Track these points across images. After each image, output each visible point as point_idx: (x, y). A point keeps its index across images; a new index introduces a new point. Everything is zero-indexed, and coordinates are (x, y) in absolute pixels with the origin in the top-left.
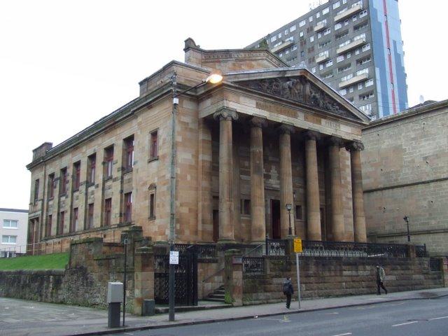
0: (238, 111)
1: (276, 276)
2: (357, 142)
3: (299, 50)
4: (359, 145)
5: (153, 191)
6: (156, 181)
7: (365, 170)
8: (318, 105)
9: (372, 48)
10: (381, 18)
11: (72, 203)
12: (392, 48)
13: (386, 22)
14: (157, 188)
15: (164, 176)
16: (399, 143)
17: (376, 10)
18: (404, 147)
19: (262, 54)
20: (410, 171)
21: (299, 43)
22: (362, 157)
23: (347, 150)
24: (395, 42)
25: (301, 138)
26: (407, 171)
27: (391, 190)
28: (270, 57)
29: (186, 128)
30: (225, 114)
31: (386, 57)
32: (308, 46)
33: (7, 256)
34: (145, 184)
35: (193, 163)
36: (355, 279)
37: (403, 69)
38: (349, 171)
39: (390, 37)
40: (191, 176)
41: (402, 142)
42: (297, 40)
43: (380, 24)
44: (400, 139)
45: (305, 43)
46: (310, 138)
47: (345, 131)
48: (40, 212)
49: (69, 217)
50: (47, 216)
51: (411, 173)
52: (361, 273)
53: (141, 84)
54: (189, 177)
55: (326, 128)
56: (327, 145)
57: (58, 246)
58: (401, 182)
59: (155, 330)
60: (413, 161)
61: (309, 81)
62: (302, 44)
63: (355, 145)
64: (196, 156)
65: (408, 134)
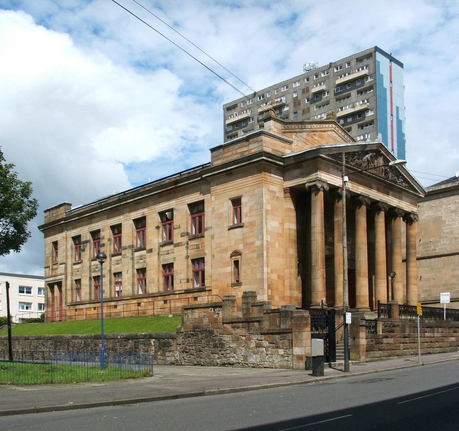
0: (328, 182)
1: (387, 337)
2: (414, 214)
3: (292, 111)
4: (415, 216)
5: (238, 257)
6: (240, 247)
7: (415, 241)
8: (388, 178)
9: (376, 113)
10: (386, 84)
11: (110, 267)
12: (395, 114)
13: (391, 88)
14: (242, 255)
15: (253, 243)
16: (439, 214)
17: (382, 76)
18: (443, 219)
19: (330, 125)
20: (448, 243)
21: (292, 104)
22: (415, 229)
23: (404, 221)
24: (397, 108)
25: (374, 207)
26: (445, 242)
27: (428, 260)
28: (337, 129)
29: (274, 197)
30: (319, 185)
31: (389, 123)
32: (302, 107)
33: (2, 318)
34: (226, 250)
35: (280, 232)
36: (432, 339)
37: (403, 135)
38: (404, 240)
39: (393, 103)
40: (279, 244)
41: (442, 213)
42: (290, 101)
43: (385, 89)
44: (440, 211)
45: (299, 104)
46: (379, 210)
47: (405, 205)
48: (63, 277)
49: (108, 283)
50: (72, 281)
51: (449, 244)
52: (436, 334)
53: (213, 150)
54: (277, 245)
55: (393, 201)
56: (392, 213)
57: (93, 312)
58: (439, 252)
59: (111, 400)
60: (452, 232)
61: (383, 155)
62: (295, 106)
63: (412, 216)
64: (282, 224)
65: (449, 206)
